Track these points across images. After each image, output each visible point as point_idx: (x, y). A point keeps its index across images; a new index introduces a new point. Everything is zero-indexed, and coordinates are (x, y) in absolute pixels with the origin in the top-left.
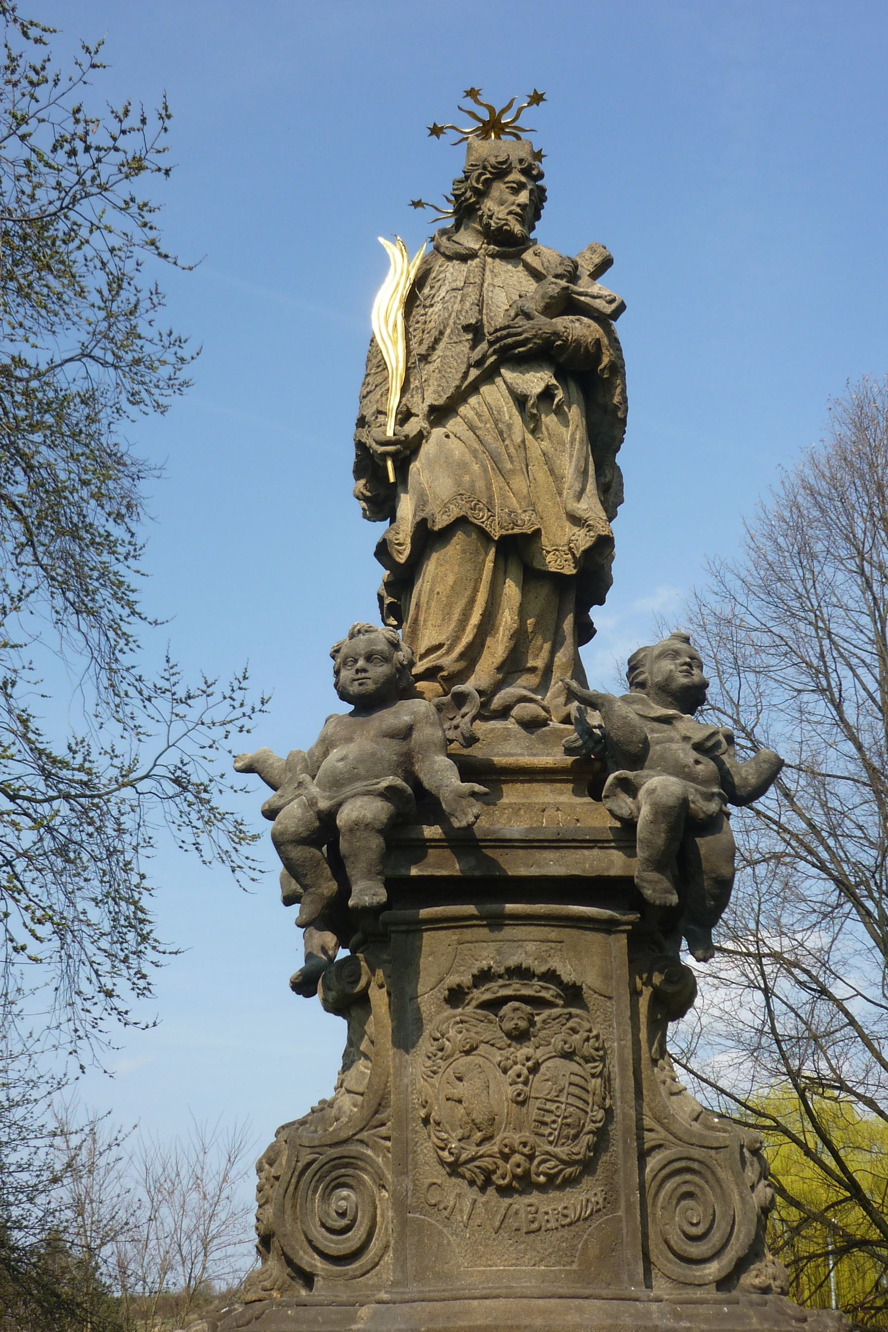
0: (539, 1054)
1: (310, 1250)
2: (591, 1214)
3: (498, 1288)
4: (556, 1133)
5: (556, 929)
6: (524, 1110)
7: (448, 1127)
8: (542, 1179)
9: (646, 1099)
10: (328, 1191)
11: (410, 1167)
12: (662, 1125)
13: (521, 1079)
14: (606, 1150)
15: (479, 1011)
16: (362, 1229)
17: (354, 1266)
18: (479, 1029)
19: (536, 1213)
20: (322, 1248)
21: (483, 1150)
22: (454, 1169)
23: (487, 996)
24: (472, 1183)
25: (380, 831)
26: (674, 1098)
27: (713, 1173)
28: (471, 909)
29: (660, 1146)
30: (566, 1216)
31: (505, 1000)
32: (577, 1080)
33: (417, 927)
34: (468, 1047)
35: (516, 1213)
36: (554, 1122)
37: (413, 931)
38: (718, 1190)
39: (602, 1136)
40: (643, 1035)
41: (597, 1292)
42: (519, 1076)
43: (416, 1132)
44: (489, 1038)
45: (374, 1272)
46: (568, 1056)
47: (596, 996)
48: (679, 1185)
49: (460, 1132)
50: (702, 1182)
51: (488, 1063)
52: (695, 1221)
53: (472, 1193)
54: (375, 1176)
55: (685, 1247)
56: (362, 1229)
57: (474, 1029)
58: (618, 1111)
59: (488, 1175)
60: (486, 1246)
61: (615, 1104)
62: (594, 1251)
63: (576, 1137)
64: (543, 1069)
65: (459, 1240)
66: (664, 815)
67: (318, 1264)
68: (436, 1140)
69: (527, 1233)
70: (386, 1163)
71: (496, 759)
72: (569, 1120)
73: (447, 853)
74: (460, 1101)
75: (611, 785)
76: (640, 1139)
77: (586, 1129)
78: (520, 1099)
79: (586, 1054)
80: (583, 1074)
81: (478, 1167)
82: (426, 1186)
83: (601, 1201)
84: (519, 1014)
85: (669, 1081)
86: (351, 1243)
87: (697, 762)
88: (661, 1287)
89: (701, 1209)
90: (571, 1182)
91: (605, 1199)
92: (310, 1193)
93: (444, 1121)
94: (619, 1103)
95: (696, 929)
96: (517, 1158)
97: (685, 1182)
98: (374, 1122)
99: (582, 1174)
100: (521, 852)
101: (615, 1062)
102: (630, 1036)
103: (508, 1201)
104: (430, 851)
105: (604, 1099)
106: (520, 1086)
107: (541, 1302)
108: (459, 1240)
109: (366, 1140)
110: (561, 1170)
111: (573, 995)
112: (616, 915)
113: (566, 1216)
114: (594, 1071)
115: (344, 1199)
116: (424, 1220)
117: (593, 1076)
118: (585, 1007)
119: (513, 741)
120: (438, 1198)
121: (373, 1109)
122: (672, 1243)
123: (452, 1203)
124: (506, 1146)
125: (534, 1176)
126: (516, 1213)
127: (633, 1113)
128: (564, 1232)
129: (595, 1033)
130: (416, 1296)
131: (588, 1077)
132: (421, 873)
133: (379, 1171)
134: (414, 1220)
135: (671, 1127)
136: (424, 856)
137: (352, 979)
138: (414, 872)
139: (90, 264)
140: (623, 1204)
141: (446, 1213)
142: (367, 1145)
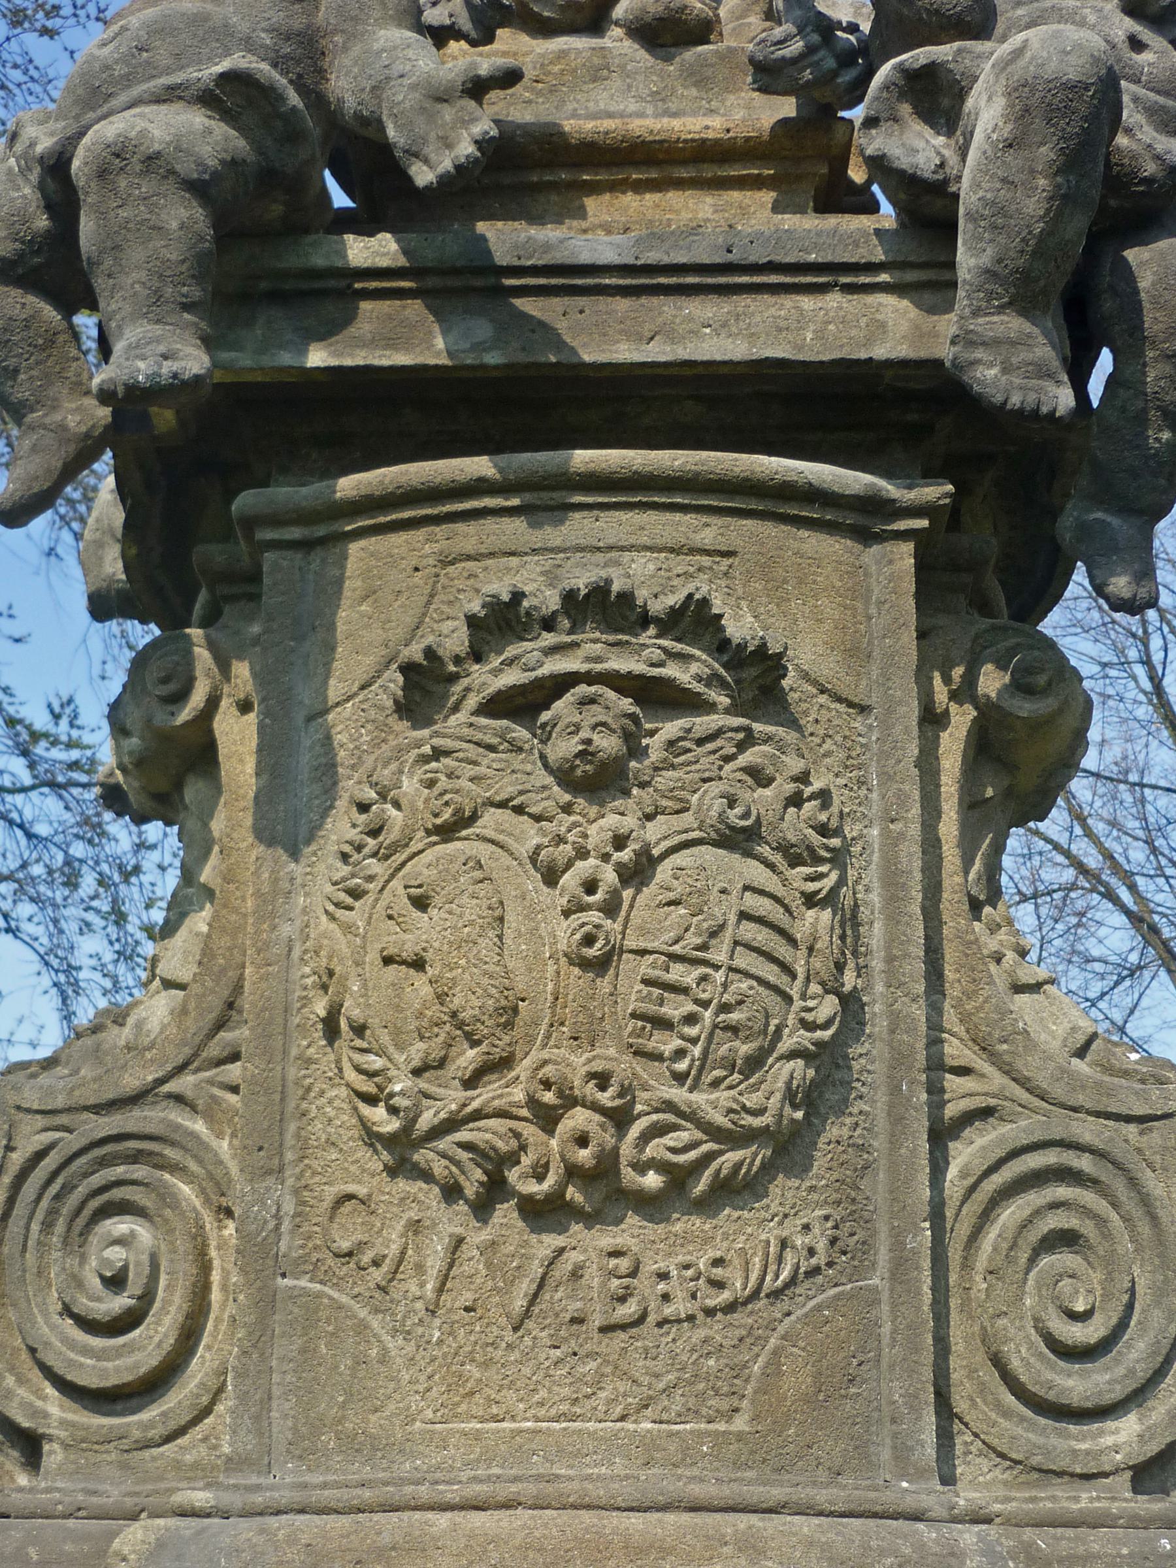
1: (36, 1375)
2: (792, 1282)
3: (516, 1479)
4: (697, 1051)
5: (717, 521)
6: (604, 985)
7: (385, 1038)
8: (653, 1180)
9: (953, 991)
10: (81, 1221)
11: (289, 1156)
13: (599, 896)
14: (841, 1108)
15: (483, 721)
16: (167, 1320)
17: (144, 1416)
18: (481, 770)
19: (633, 1274)
20: (60, 1368)
21: (481, 1097)
23: (512, 677)
24: (451, 1192)
25: (199, 188)
26: (1023, 999)
27: (1133, 1182)
28: (480, 466)
29: (986, 1113)
30: (719, 1285)
31: (562, 684)
32: (762, 906)
33: (328, 530)
34: (447, 815)
35: (576, 1274)
36: (691, 1019)
37: (322, 541)
38: (1145, 1229)
39: (830, 1060)
40: (949, 827)
41: (803, 1494)
43: (309, 1061)
44: (511, 790)
45: (197, 1432)
46: (739, 839)
47: (823, 699)
48: (1037, 1213)
49: (417, 1051)
50: (1100, 1205)
51: (506, 860)
52: (1080, 1307)
53: (453, 1220)
54: (209, 1186)
55: (1049, 1375)
56: (167, 1320)
58: (876, 1009)
59: (496, 1167)
60: (486, 1364)
61: (868, 987)
62: (796, 1381)
63: (755, 1063)
64: (663, 873)
65: (410, 1348)
66: (1051, 113)
67: (55, 1411)
68: (351, 1075)
71: (568, 126)
72: (735, 1016)
73: (415, 309)
74: (418, 964)
75: (886, 87)
76: (935, 1090)
77: (784, 1046)
78: (592, 952)
79: (792, 837)
80: (780, 891)
81: (467, 1146)
82: (327, 1203)
83: (821, 1246)
84: (596, 713)
85: (1010, 956)
86: (137, 1356)
87: (1136, 44)
88: (979, 1482)
89: (1097, 1276)
90: (733, 1190)
91: (833, 1241)
92: (35, 1227)
93: (374, 1022)
94: (879, 988)
95: (1115, 521)
96: (578, 1119)
97: (1055, 1205)
98: (214, 1050)
99: (769, 1169)
100: (622, 304)
101: (872, 876)
102: (916, 811)
103: (552, 1241)
104: (365, 306)
105: (840, 967)
106: (595, 916)
107: (635, 1521)
108: (410, 1348)
109: (189, 1094)
110: (710, 1157)
111: (758, 679)
112: (889, 489)
113: (719, 1285)
114: (811, 887)
115: (120, 1241)
116: (319, 1295)
117: (810, 900)
118: (793, 724)
119: (616, 82)
120: (359, 1237)
121: (211, 1017)
122: (1015, 1364)
123: (394, 1249)
124: (547, 1084)
125: (628, 1175)
126: (576, 1274)
127: (919, 1012)
128: (714, 1329)
129: (817, 785)
130: (285, 1497)
131: (796, 903)
132: (334, 362)
133: (218, 1172)
134: (294, 1295)
135: (1019, 1064)
136: (349, 318)
137: (172, 687)
138: (317, 357)
139: (81, 13)
140: (883, 1255)
141: (377, 1275)
142: (194, 1108)
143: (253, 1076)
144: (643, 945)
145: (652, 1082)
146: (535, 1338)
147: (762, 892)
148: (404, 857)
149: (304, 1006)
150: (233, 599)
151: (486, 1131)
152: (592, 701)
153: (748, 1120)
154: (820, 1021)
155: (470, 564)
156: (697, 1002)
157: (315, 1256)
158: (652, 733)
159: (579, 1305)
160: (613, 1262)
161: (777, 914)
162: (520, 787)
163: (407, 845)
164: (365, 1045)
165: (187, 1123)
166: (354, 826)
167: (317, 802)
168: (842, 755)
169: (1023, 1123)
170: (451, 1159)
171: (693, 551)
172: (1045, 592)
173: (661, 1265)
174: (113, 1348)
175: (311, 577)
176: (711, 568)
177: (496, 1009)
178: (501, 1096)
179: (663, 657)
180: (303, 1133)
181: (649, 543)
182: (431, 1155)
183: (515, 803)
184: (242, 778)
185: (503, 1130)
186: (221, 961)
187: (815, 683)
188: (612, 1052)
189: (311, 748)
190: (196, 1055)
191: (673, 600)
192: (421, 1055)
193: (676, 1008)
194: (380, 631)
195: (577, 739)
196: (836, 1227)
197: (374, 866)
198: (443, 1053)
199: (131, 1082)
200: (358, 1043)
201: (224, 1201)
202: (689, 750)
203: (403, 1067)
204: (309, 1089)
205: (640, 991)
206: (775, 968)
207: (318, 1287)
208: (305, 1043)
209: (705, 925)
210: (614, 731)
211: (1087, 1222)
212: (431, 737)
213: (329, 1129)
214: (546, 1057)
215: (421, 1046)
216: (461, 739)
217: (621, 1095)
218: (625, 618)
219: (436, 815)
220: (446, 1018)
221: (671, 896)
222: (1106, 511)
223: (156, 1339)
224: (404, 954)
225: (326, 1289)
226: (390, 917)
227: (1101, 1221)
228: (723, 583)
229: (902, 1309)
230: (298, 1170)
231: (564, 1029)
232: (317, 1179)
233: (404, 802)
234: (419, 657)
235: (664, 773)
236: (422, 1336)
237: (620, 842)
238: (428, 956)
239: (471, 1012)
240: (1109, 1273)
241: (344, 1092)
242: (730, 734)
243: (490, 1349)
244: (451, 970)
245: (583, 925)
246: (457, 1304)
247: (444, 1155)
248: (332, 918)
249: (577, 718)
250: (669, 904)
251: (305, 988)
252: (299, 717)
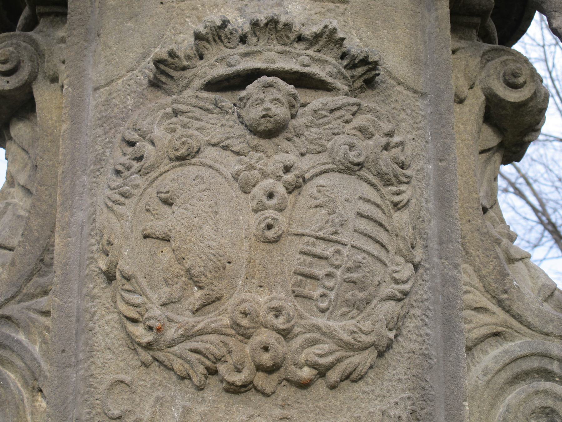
0: (306, 165)
4: (332, 295)
11: (81, 356)
12: (500, 303)
13: (274, 201)
15: (205, 94)
18: (203, 124)
23: (221, 70)
42: (271, 196)
43: (94, 297)
46: (352, 168)
47: (399, 88)
49: (165, 292)
51: (219, 179)
54: (27, 373)
64: (310, 189)
68: (123, 307)
74: (166, 239)
78: (270, 234)
80: (379, 201)
106: (271, 213)
110: (339, 360)
111: (365, 73)
114: (396, 199)
124: (245, 314)
143: (59, 306)
144: (300, 231)
145: (306, 314)
148: (156, 174)
149: (92, 263)
150: (42, 15)
151: (206, 342)
154: (405, 278)
156: (333, 265)
158: (304, 105)
161: (378, 214)
162: (227, 135)
164: (131, 288)
165: (13, 335)
166: (124, 154)
167: (100, 139)
169: (518, 342)
170: (184, 359)
172: (517, 29)
178: (215, 321)
180: (90, 342)
183: (224, 144)
184: (50, 122)
185: (218, 342)
186: (36, 234)
187: (395, 79)
188: (283, 295)
189: (96, 106)
190: (19, 292)
191: (317, 29)
193: (320, 270)
195: (261, 108)
196: (413, 404)
198: (180, 294)
200: (128, 287)
201: (36, 384)
202: (325, 116)
203: (155, 302)
204: (94, 315)
205: (298, 259)
208: (91, 286)
210: (283, 104)
212: (173, 103)
213: (107, 340)
214: (244, 297)
215: (167, 289)
218: (288, 37)
219: (177, 150)
220: (182, 273)
221: (317, 202)
224: (157, 233)
226: (148, 210)
230: (86, 365)
232: (98, 371)
233: (156, 141)
235: (312, 129)
238: (173, 234)
239: (198, 269)
242: (348, 108)
245: (266, 218)
247: (181, 357)
248: (111, 210)
249: (262, 96)
250: (317, 206)
251: (92, 252)
252: (90, 87)
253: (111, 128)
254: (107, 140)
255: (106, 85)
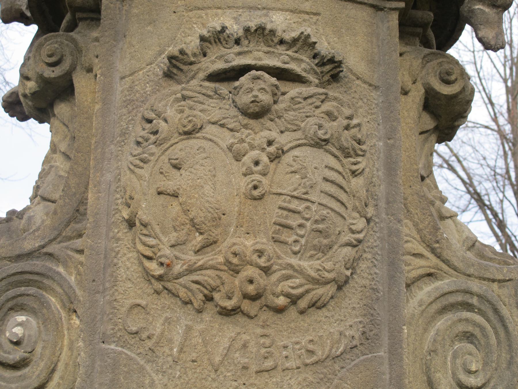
0: (284, 140)
8: (282, 301)
11: (107, 285)
12: (433, 251)
13: (259, 168)
15: (207, 84)
18: (205, 107)
22: (163, 282)
23: (220, 65)
27: (496, 311)
36: (301, 226)
42: (257, 163)
43: (118, 239)
46: (320, 143)
47: (358, 82)
49: (173, 237)
51: (217, 149)
53: (184, 318)
54: (65, 298)
57: (200, 107)
64: (287, 158)
65: (165, 380)
69: (257, 372)
70: (80, 283)
74: (175, 196)
78: (256, 193)
80: (341, 169)
81: (197, 282)
83: (357, 335)
93: (154, 223)
95: (487, 10)
96: (250, 272)
98: (68, 232)
110: (307, 292)
111: (332, 70)
113: (311, 352)
114: (354, 168)
115: (20, 324)
116: (121, 353)
120: (142, 324)
123: (159, 330)
124: (235, 254)
126: (245, 346)
140: (385, 340)
144: (279, 191)
145: (282, 255)
146: (225, 376)
147: (332, 169)
148: (168, 145)
151: (205, 276)
152: (258, 78)
153: (327, 275)
155: (199, 12)
156: (304, 218)
157: (119, 334)
158: (284, 94)
159: (246, 360)
160: (262, 340)
161: (339, 179)
162: (224, 116)
163: (170, 140)
164: (147, 233)
165: (55, 268)
166: (144, 129)
167: (125, 117)
168: (367, 108)
169: (447, 281)
171: (301, 12)
172: (451, 37)
173: (285, 342)
174: (14, 377)
175: (124, 12)
176: (309, 20)
177: (212, 218)
178: (212, 259)
179: (289, 59)
180: (114, 274)
181: (281, 7)
182: (178, 286)
183: (221, 122)
185: (214, 275)
186: (74, 190)
188: (265, 240)
189: (122, 92)
190: (59, 234)
192: (175, 238)
194: (157, 39)
195: (251, 95)
196: (364, 327)
197: (153, 148)
198: (185, 238)
199: (28, 245)
200: (145, 232)
201: (72, 306)
202: (300, 103)
204: (118, 253)
206: (339, 204)
207: (120, 349)
209: (308, 183)
210: (268, 93)
211: (476, 328)
212: (182, 90)
213: (128, 273)
214: (235, 241)
215: (175, 234)
216: (196, 92)
217: (268, 261)
218: (272, 41)
219: (185, 127)
220: (187, 222)
221: (293, 169)
222: (483, 5)
223: (37, 373)
224: (168, 191)
225: (124, 350)
226: (161, 173)
227: (482, 329)
228: (314, 27)
229: (394, 367)
230: (111, 292)
231: (242, 229)
233: (169, 119)
234: (177, 53)
236: (171, 374)
237: (270, 143)
238: (181, 192)
239: (200, 219)
240: (487, 353)
241: (135, 255)
243: (203, 381)
244: (191, 199)
245: (253, 181)
246: (188, 359)
247: (185, 287)
248: (132, 172)
249: (252, 86)
251: (117, 205)
252: (117, 76)
253: (133, 109)
254: (130, 118)
255: (131, 75)
